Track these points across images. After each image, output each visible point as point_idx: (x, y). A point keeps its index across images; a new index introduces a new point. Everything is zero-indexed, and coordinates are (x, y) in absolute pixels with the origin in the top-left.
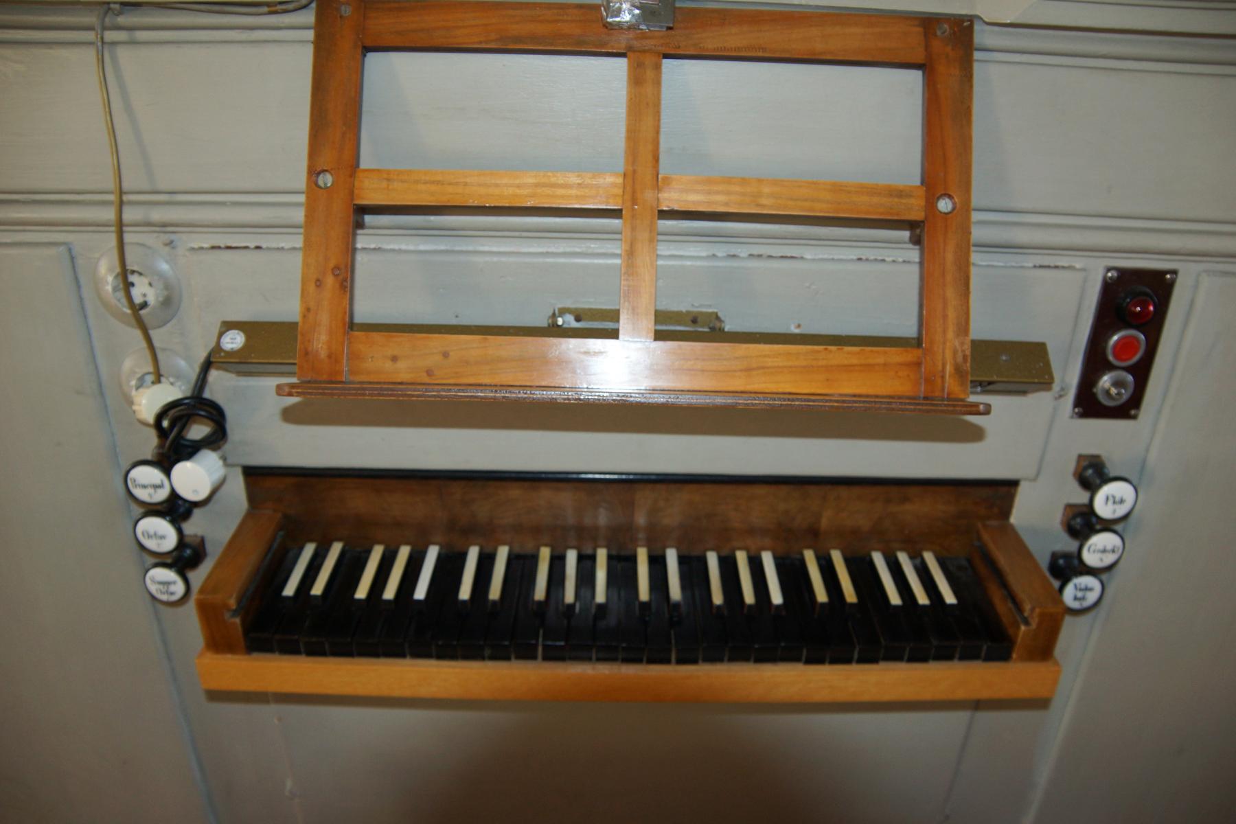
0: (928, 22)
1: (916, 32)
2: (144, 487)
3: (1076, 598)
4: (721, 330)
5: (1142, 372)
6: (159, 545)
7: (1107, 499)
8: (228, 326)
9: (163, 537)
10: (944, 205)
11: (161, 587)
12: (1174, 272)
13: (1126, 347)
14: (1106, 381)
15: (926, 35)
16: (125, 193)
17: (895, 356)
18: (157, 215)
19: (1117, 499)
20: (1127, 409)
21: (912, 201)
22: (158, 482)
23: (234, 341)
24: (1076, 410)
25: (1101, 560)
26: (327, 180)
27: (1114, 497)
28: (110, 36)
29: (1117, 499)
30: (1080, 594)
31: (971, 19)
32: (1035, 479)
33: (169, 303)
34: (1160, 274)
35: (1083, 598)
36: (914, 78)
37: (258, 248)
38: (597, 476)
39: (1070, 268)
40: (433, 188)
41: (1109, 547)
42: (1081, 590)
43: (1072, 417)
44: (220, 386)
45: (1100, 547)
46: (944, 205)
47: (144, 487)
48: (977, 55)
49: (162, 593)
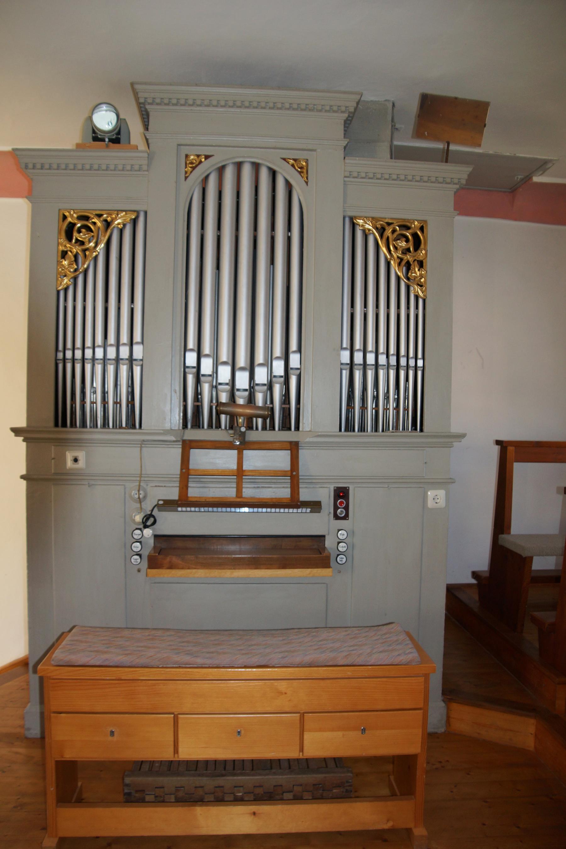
0: (291, 442)
1: (288, 445)
2: (136, 535)
3: (340, 561)
4: (97, 137)
5: (347, 508)
6: (137, 549)
7: (340, 534)
8: (159, 500)
9: (138, 547)
10: (294, 473)
11: (135, 560)
12: (349, 487)
13: (341, 503)
14: (339, 511)
15: (290, 444)
16: (283, 474)
17: (244, 475)
18: (146, 479)
19: (343, 534)
20: (346, 517)
21: (288, 473)
22: (140, 534)
23: (161, 502)
24: (334, 518)
25: (343, 549)
26: (184, 471)
27: (342, 534)
28: (143, 446)
29: (343, 534)
30: (341, 559)
31: (298, 442)
32: (328, 534)
33: (145, 497)
34: (345, 488)
35: (342, 561)
36: (289, 451)
37: (165, 486)
38: (232, 536)
39: (327, 487)
40: (203, 472)
41: (344, 546)
42: (341, 558)
43: (334, 520)
44: (155, 512)
45: (342, 546)
46: (294, 473)
47: (136, 535)
48: (300, 448)
49: (135, 562)
